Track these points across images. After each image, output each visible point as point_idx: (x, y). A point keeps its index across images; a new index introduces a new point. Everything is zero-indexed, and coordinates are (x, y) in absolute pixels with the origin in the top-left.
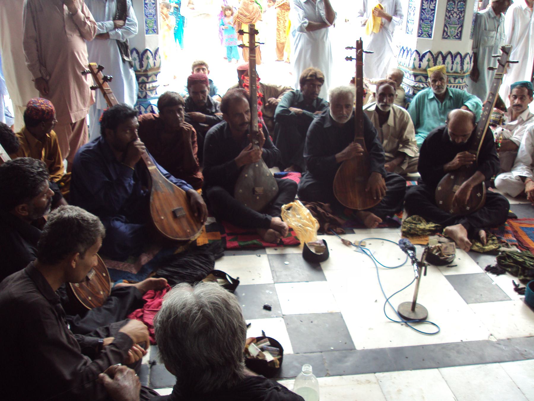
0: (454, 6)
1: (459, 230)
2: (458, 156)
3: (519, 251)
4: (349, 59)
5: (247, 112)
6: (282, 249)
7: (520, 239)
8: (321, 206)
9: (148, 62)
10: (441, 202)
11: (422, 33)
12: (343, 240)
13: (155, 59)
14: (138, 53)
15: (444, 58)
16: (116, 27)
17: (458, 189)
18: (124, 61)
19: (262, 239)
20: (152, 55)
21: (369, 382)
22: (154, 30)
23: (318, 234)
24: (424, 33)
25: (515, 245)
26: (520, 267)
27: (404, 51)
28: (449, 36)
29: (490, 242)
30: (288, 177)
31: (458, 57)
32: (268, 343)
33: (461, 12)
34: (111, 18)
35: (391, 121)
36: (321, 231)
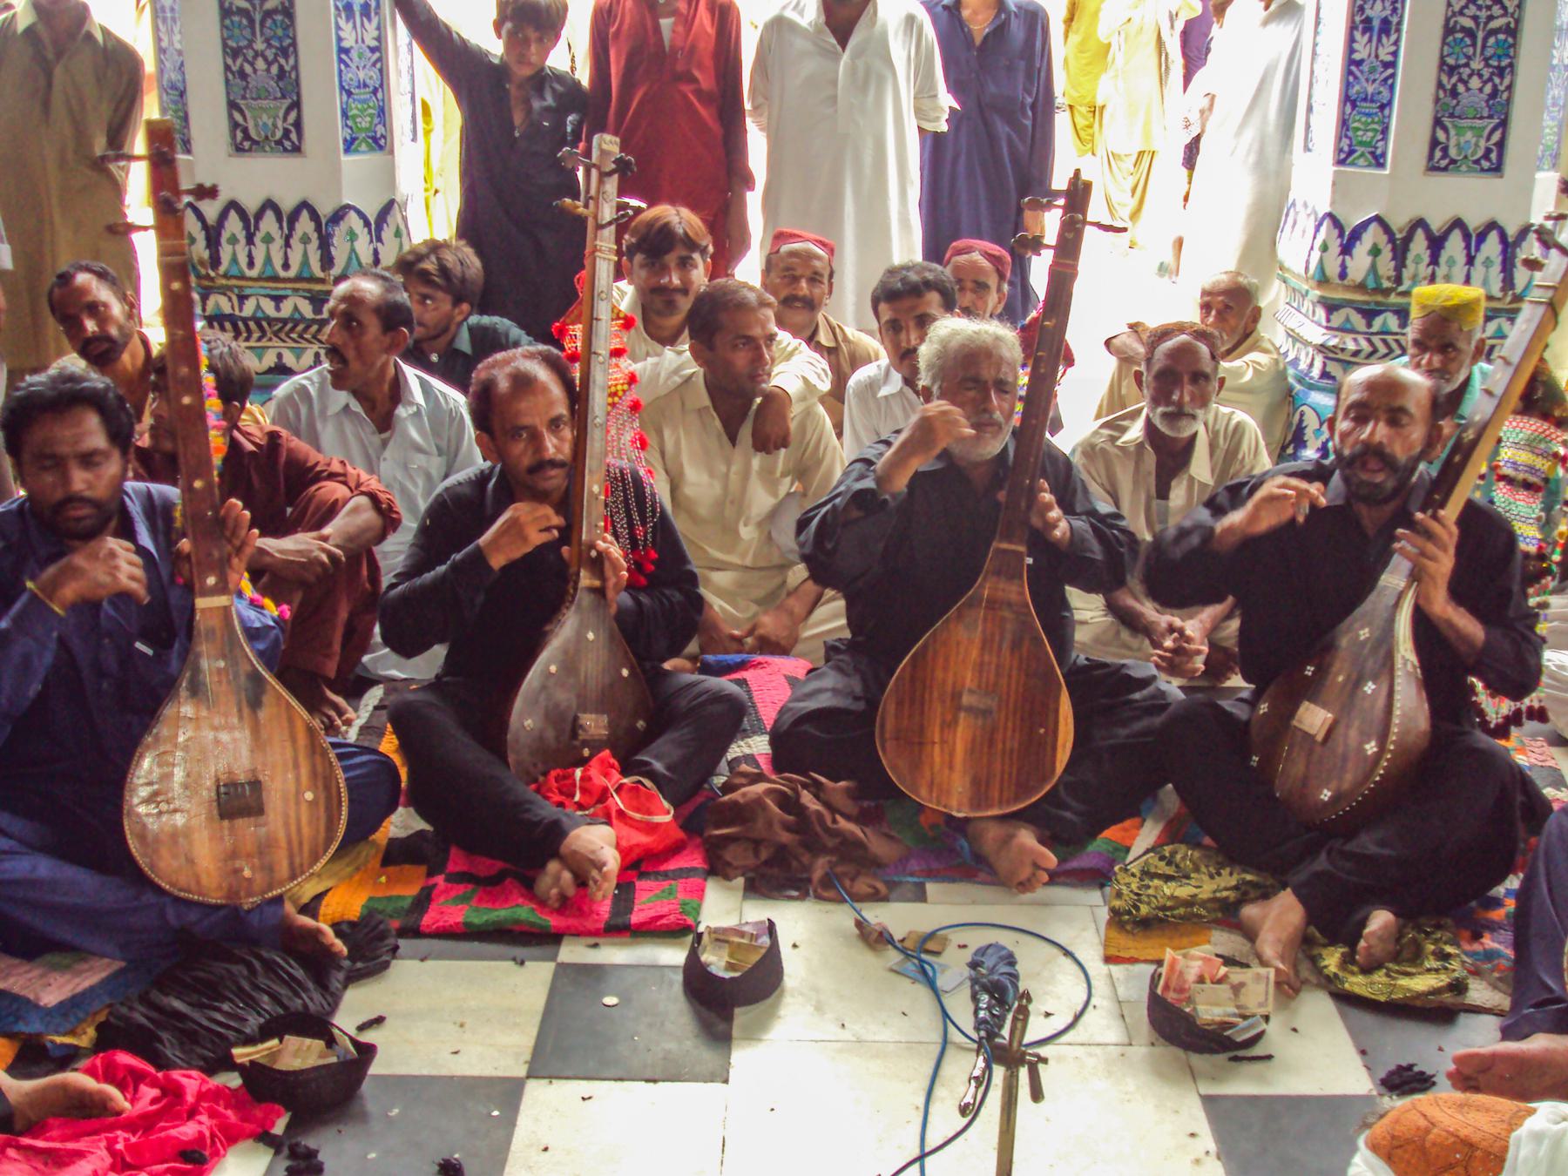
9: (353, 250)
11: (1351, 152)
13: (379, 239)
20: (367, 224)
24: (1360, 150)
28: (1453, 162)
31: (1493, 237)
33: (1500, 72)
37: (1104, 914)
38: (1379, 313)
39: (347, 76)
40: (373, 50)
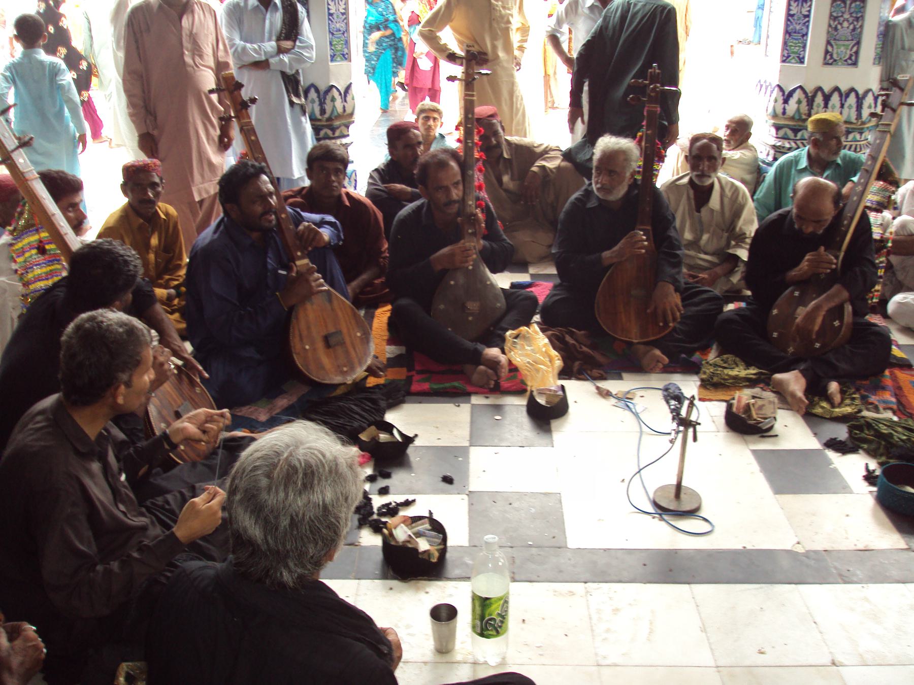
0: (843, 10)
1: (794, 381)
2: (807, 258)
3: (895, 419)
5: (456, 184)
6: (497, 398)
7: (903, 400)
8: (572, 334)
9: (334, 106)
10: (775, 335)
11: (788, 57)
12: (598, 388)
13: (346, 101)
14: (317, 91)
15: (827, 98)
16: (280, 51)
17: (801, 312)
18: (292, 103)
19: (469, 381)
20: (340, 94)
21: (572, 593)
22: (343, 55)
23: (560, 379)
24: (793, 55)
25: (891, 409)
26: (883, 443)
27: (761, 86)
28: (835, 61)
29: (848, 401)
30: (532, 289)
31: (853, 95)
32: (427, 526)
33: (857, 19)
34: (274, 38)
35: (715, 201)
36: (565, 373)
37: (699, 383)
38: (800, 130)
39: (332, 26)
40: (343, 14)
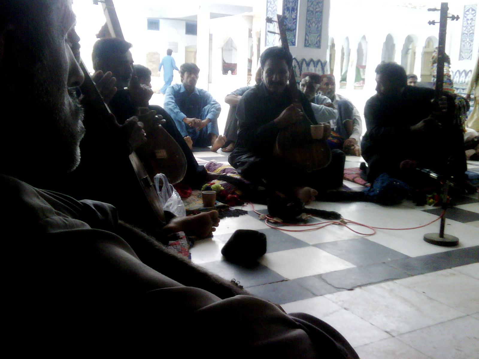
4: (433, 23)
28: (310, 44)
